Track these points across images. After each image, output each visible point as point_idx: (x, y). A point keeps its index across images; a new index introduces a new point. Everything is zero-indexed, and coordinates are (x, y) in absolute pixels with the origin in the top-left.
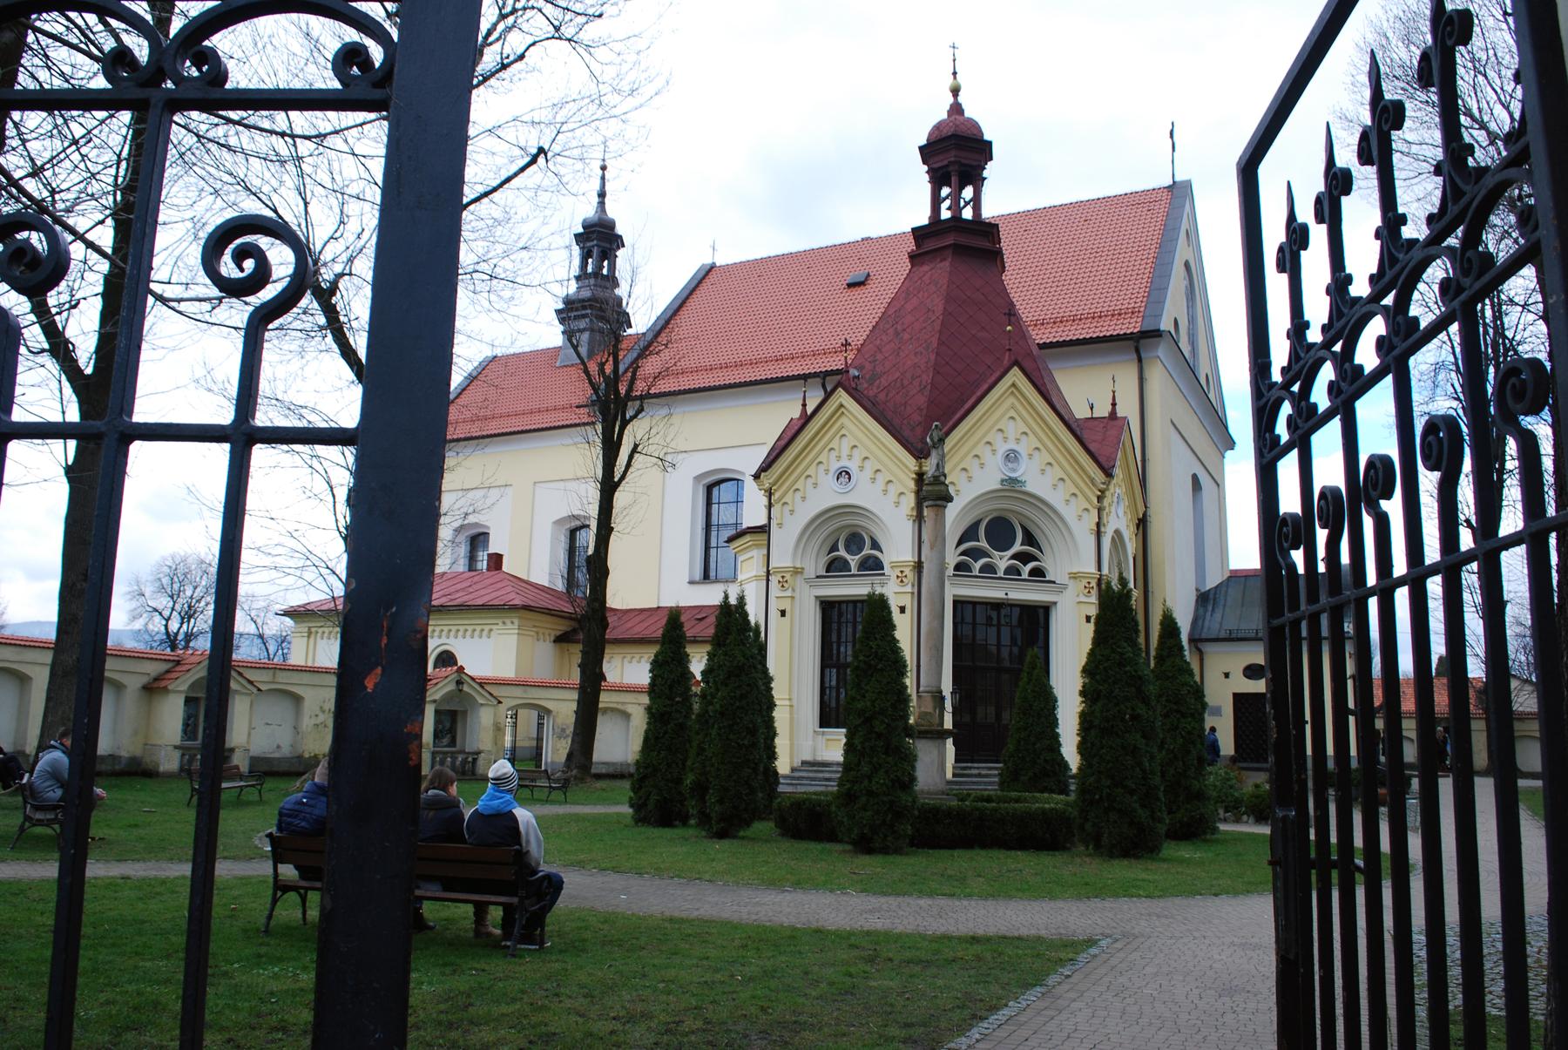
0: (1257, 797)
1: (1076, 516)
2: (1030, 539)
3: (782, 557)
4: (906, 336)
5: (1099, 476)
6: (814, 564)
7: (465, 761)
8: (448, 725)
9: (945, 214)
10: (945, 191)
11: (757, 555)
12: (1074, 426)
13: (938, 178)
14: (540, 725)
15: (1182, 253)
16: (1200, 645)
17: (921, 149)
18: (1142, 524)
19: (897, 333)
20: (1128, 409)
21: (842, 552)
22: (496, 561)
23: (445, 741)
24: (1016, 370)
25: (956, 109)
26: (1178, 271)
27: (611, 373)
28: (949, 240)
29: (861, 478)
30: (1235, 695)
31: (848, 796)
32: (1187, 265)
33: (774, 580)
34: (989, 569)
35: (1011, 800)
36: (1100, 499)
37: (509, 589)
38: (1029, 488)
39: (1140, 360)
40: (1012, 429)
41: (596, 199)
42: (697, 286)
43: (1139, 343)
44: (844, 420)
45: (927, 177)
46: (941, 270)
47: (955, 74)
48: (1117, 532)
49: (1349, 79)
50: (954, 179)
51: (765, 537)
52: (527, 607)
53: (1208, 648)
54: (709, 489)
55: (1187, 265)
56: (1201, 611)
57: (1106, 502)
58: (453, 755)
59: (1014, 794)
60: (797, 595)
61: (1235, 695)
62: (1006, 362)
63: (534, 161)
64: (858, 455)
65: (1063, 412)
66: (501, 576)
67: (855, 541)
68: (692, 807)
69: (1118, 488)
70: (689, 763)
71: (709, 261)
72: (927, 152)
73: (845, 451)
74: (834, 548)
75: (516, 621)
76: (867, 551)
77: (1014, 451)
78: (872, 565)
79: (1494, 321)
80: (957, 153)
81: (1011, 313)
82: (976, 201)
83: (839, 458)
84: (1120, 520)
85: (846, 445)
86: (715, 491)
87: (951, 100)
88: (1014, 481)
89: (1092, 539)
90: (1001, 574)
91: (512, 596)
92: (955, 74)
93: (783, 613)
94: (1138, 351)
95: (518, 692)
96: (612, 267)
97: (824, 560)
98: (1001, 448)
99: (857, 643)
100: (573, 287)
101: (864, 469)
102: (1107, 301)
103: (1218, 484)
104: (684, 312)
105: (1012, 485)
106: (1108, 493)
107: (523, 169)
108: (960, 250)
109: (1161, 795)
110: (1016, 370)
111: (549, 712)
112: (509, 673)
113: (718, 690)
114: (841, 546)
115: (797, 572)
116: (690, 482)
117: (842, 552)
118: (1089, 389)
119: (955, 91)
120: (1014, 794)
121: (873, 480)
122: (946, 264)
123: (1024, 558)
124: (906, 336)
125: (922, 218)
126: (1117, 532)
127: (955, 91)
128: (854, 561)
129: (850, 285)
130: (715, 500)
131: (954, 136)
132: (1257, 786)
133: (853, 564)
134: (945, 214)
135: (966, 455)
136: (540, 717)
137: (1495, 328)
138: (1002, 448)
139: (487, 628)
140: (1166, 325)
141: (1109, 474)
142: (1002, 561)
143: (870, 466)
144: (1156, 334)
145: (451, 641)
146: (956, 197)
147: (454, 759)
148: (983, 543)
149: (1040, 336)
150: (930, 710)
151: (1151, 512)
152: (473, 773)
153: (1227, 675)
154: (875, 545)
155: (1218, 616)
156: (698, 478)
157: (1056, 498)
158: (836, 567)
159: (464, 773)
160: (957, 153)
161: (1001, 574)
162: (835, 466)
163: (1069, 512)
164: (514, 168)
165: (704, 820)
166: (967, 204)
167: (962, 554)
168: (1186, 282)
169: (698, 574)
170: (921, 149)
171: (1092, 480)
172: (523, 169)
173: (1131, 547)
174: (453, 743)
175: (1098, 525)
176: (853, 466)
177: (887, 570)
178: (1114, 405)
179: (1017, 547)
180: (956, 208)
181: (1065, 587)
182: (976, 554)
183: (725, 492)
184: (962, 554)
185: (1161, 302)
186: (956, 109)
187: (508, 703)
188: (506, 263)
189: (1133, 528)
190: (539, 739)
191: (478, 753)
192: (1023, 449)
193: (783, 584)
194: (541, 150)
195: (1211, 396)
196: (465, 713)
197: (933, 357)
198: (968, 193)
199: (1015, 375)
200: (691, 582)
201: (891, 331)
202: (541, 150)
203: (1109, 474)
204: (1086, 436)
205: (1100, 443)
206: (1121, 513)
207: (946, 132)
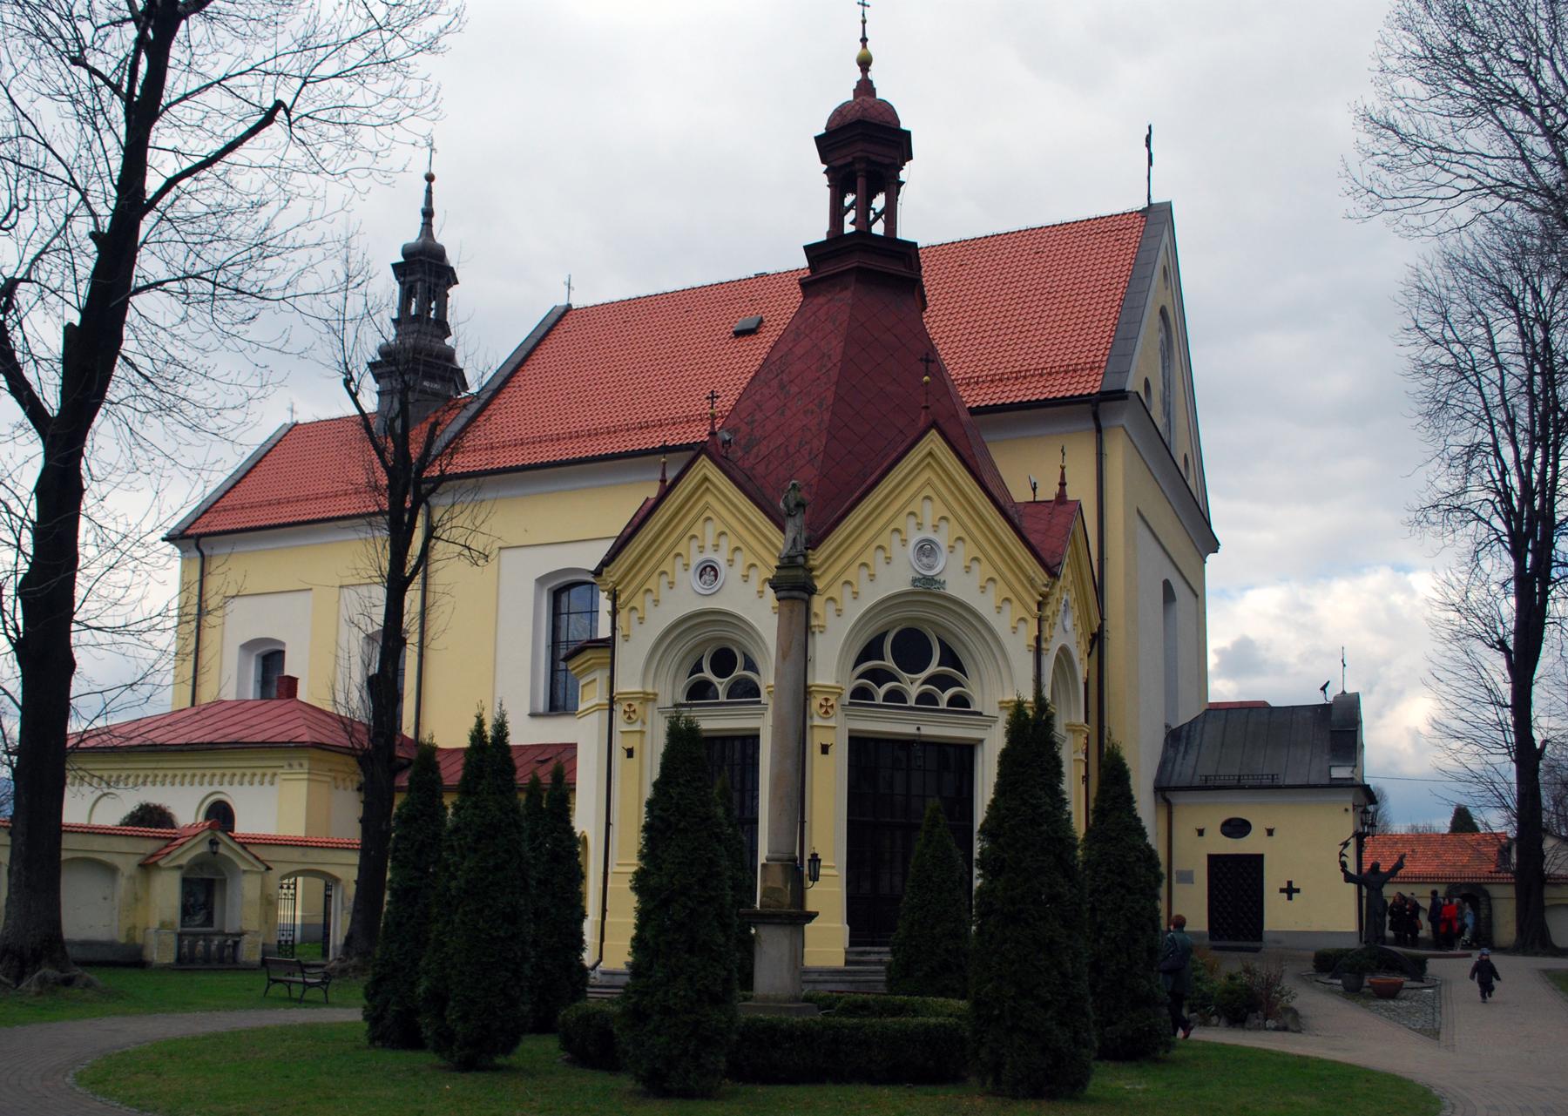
0: (1231, 993)
1: (1012, 630)
2: (950, 658)
3: (628, 683)
4: (794, 389)
5: (1041, 577)
6: (671, 690)
7: (221, 947)
8: (202, 898)
9: (849, 228)
10: (849, 199)
11: (601, 676)
12: (1011, 512)
13: (840, 182)
14: (327, 897)
15: (1156, 296)
16: (1168, 795)
17: (818, 139)
18: (1097, 640)
19: (782, 386)
20: (1081, 490)
21: (708, 674)
22: (291, 685)
23: (199, 918)
24: (933, 434)
25: (865, 88)
26: (1151, 318)
27: (418, 435)
28: (852, 263)
29: (730, 575)
30: (1211, 857)
31: (637, 1015)
32: (1163, 312)
33: (619, 710)
34: (896, 696)
35: (899, 1010)
36: (1040, 605)
37: (301, 721)
38: (951, 590)
39: (1099, 430)
40: (929, 513)
41: (420, 219)
42: (547, 334)
43: (1097, 408)
44: (709, 498)
45: (825, 180)
46: (841, 303)
47: (864, 40)
48: (1064, 650)
49: (1376, 65)
50: (861, 182)
51: (607, 653)
52: (314, 746)
53: (1178, 799)
54: (557, 595)
55: (1163, 312)
56: (1171, 752)
57: (1048, 612)
58: (207, 937)
59: (901, 998)
60: (648, 728)
61: (1211, 857)
62: (921, 423)
63: (269, 118)
64: (726, 544)
65: (996, 493)
66: (293, 705)
67: (724, 661)
68: (427, 1025)
69: (1066, 591)
70: (422, 963)
71: (563, 302)
72: (827, 144)
73: (710, 540)
74: (698, 668)
75: (306, 764)
76: (739, 672)
77: (930, 541)
78: (747, 691)
79: (1544, 391)
80: (865, 147)
81: (930, 359)
82: (890, 213)
83: (701, 549)
84: (1067, 634)
85: (710, 532)
86: (564, 598)
87: (859, 76)
88: (930, 581)
89: (1030, 658)
90: (911, 702)
91: (299, 731)
92: (864, 40)
93: (630, 753)
94: (1096, 418)
95: (295, 854)
96: (442, 308)
97: (684, 683)
98: (917, 537)
99: (702, 787)
100: (391, 333)
101: (724, 562)
102: (1060, 353)
103: (1198, 594)
104: (528, 369)
105: (927, 587)
106: (1052, 600)
107: (253, 131)
108: (866, 276)
109: (1089, 1008)
110: (933, 434)
111: (337, 880)
112: (297, 830)
113: (464, 857)
114: (706, 665)
115: (648, 698)
116: (532, 586)
117: (708, 674)
118: (1032, 469)
119: (865, 63)
120: (901, 998)
121: (746, 578)
122: (847, 294)
123: (942, 681)
124: (794, 389)
125: (819, 231)
126: (1064, 650)
127: (865, 63)
128: (721, 685)
129: (739, 334)
130: (564, 609)
131: (859, 123)
132: (1232, 978)
133: (720, 689)
134: (849, 228)
135: (867, 546)
136: (327, 888)
137: (1546, 400)
138: (915, 538)
139: (269, 772)
140: (1133, 384)
141: (1053, 573)
142: (913, 686)
143: (742, 560)
144: (1120, 395)
145: (226, 788)
146: (864, 206)
147: (208, 941)
148: (889, 663)
149: (974, 398)
150: (779, 884)
151: (1109, 625)
152: (235, 960)
153: (1201, 832)
154: (750, 665)
155: (1191, 758)
156: (541, 581)
157: (984, 605)
158: (699, 691)
159: (221, 960)
160: (865, 147)
161: (911, 702)
162: (696, 559)
163: (1001, 624)
164: (243, 129)
165: (444, 1041)
166: (878, 216)
167: (859, 677)
168: (1162, 335)
169: (542, 705)
170: (818, 139)
171: (1031, 581)
172: (253, 131)
173: (1082, 668)
174: (209, 920)
175: (1038, 639)
176: (720, 559)
177: (764, 697)
178: (1063, 484)
179: (933, 668)
180: (864, 222)
181: (994, 719)
182: (879, 676)
183: (575, 599)
184: (859, 677)
185: (1128, 355)
186: (865, 88)
187: (279, 870)
188: (251, 275)
189: (1084, 646)
190: (327, 913)
191: (241, 934)
192: (942, 539)
193: (629, 715)
194: (279, 105)
195: (1191, 482)
196: (224, 882)
197: (827, 416)
198: (879, 202)
199: (933, 442)
200: (533, 715)
201: (775, 383)
202: (279, 105)
203: (1053, 573)
204: (1025, 525)
205: (1046, 537)
206: (1069, 624)
207: (850, 118)
